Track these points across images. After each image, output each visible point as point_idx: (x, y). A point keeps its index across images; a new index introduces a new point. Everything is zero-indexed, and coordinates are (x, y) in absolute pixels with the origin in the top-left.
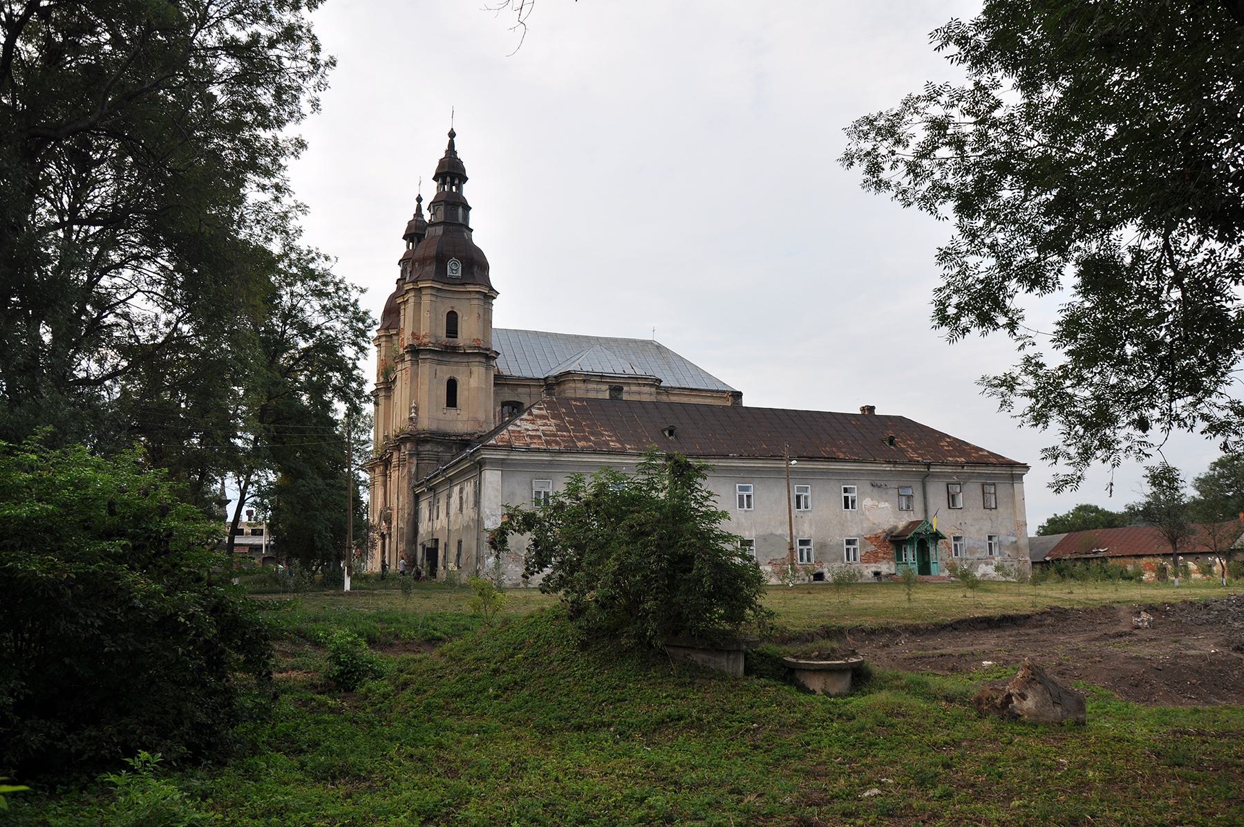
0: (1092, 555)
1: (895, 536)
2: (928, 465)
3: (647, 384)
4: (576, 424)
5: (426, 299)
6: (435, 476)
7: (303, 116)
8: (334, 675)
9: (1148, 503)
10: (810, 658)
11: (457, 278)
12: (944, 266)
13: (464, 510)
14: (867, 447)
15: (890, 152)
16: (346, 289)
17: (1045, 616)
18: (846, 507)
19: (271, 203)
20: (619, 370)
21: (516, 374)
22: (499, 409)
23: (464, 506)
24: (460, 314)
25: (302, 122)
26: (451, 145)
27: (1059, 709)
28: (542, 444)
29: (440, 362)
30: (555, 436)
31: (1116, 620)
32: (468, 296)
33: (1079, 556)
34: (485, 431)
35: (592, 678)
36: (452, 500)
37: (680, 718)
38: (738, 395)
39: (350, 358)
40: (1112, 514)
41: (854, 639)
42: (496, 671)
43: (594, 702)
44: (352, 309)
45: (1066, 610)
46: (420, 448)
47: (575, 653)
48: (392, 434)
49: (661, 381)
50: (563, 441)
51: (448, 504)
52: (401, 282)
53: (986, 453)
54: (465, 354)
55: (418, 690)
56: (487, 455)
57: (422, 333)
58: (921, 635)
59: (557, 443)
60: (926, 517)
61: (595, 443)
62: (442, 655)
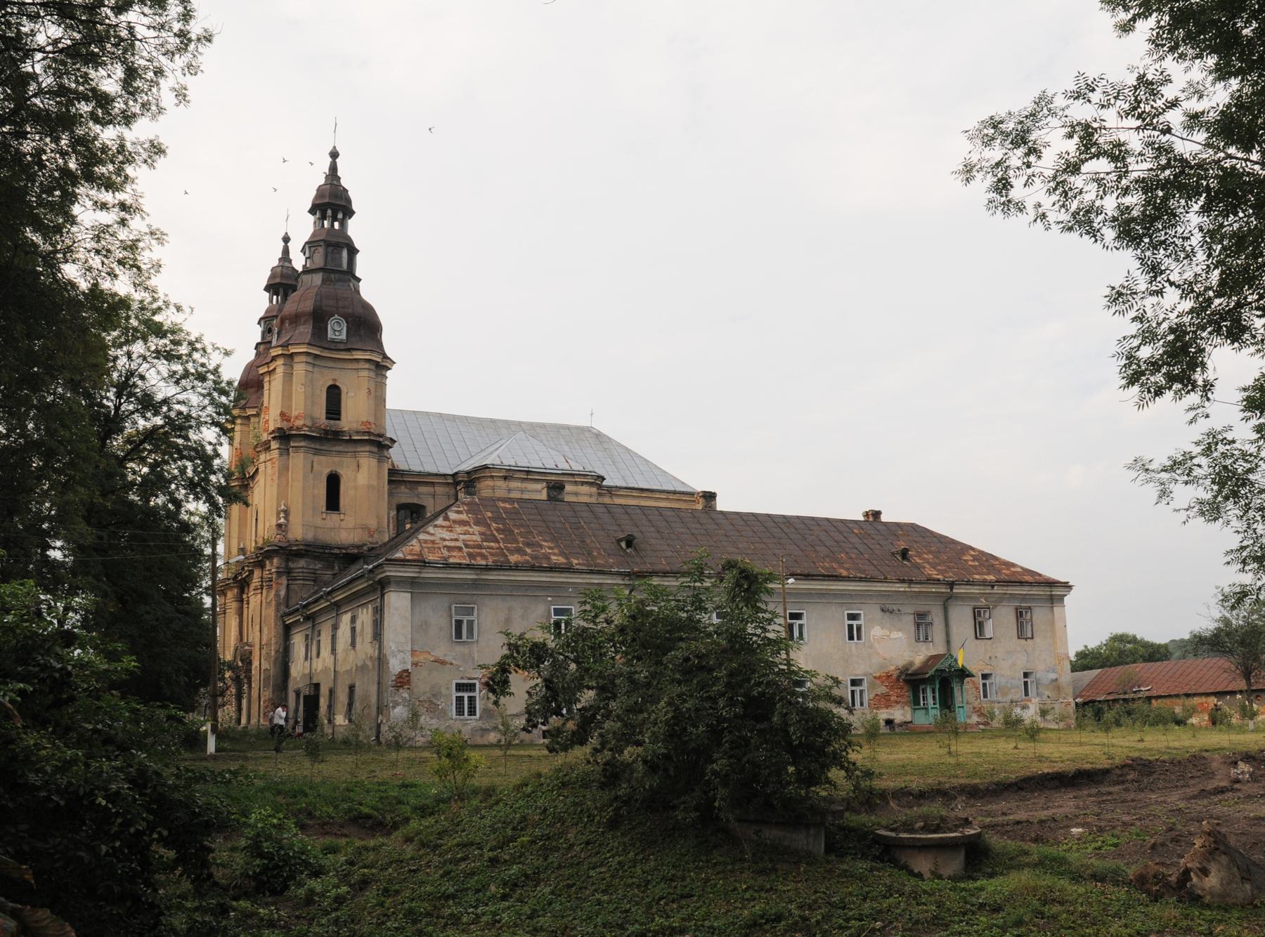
0: (1132, 696)
1: (911, 675)
2: (951, 585)
3: (587, 483)
4: (507, 531)
5: (300, 368)
6: (316, 601)
7: (161, 110)
8: (254, 872)
9: (1218, 629)
10: (912, 831)
11: (341, 342)
12: (1113, 310)
13: (358, 646)
14: (875, 562)
15: (1024, 163)
16: (204, 350)
17: (1126, 770)
18: (851, 638)
19: (116, 226)
20: (550, 464)
21: (417, 468)
22: (393, 513)
23: (358, 640)
24: (344, 389)
25: (161, 118)
26: (333, 168)
27: (1248, 886)
28: (464, 557)
29: (317, 452)
30: (480, 547)
31: (1208, 773)
32: (355, 366)
33: (1117, 697)
34: (377, 543)
35: (635, 866)
36: (340, 633)
37: (779, 918)
38: (710, 497)
39: (210, 443)
40: (1152, 645)
41: (899, 805)
42: (494, 861)
43: (648, 900)
44: (211, 377)
45: (1150, 762)
46: (291, 565)
47: (603, 833)
48: (251, 546)
49: (603, 479)
50: (492, 554)
51: (334, 638)
52: (262, 347)
53: (1019, 570)
54: (351, 441)
55: (386, 890)
56: (392, 572)
57: (294, 413)
58: (982, 798)
59: (484, 557)
60: (949, 649)
62: (408, 840)
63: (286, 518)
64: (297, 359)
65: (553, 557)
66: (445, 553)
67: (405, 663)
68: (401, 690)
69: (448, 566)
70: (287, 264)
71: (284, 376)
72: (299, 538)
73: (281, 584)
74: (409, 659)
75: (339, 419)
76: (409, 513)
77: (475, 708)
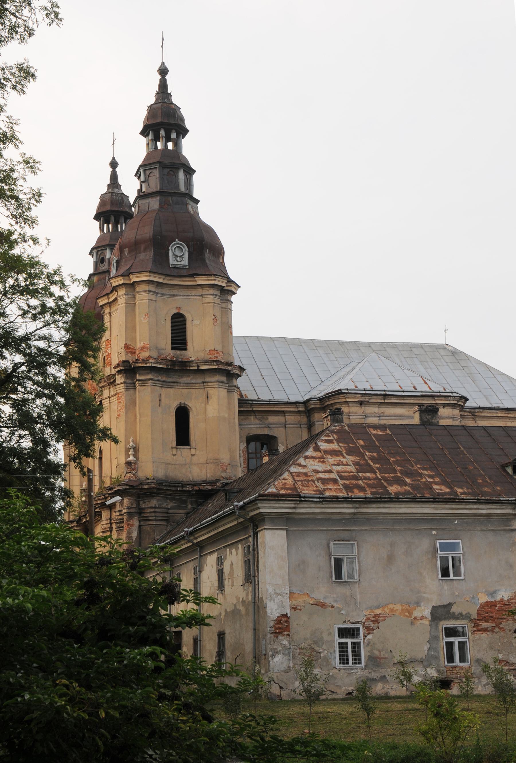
3: (448, 405)
11: (183, 268)
20: (408, 387)
21: (265, 396)
23: (227, 583)
26: (163, 85)
29: (165, 384)
30: (356, 478)
32: (199, 292)
34: (230, 478)
36: (204, 575)
49: (466, 400)
50: (369, 485)
52: (95, 278)
54: (199, 372)
56: (266, 508)
57: (139, 345)
59: (361, 489)
61: (412, 487)
63: (135, 455)
64: (139, 288)
65: (435, 487)
66: (321, 486)
67: (283, 607)
68: (280, 637)
69: (324, 500)
70: (116, 190)
71: (126, 307)
72: (150, 475)
73: (132, 525)
74: (287, 603)
75: (185, 349)
76: (259, 444)
77: (360, 655)
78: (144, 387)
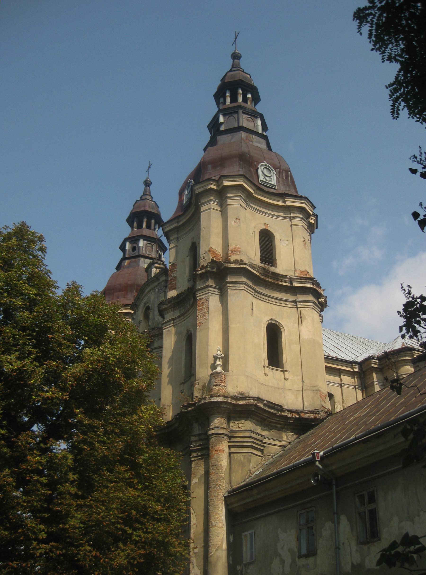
78: (235, 291)
